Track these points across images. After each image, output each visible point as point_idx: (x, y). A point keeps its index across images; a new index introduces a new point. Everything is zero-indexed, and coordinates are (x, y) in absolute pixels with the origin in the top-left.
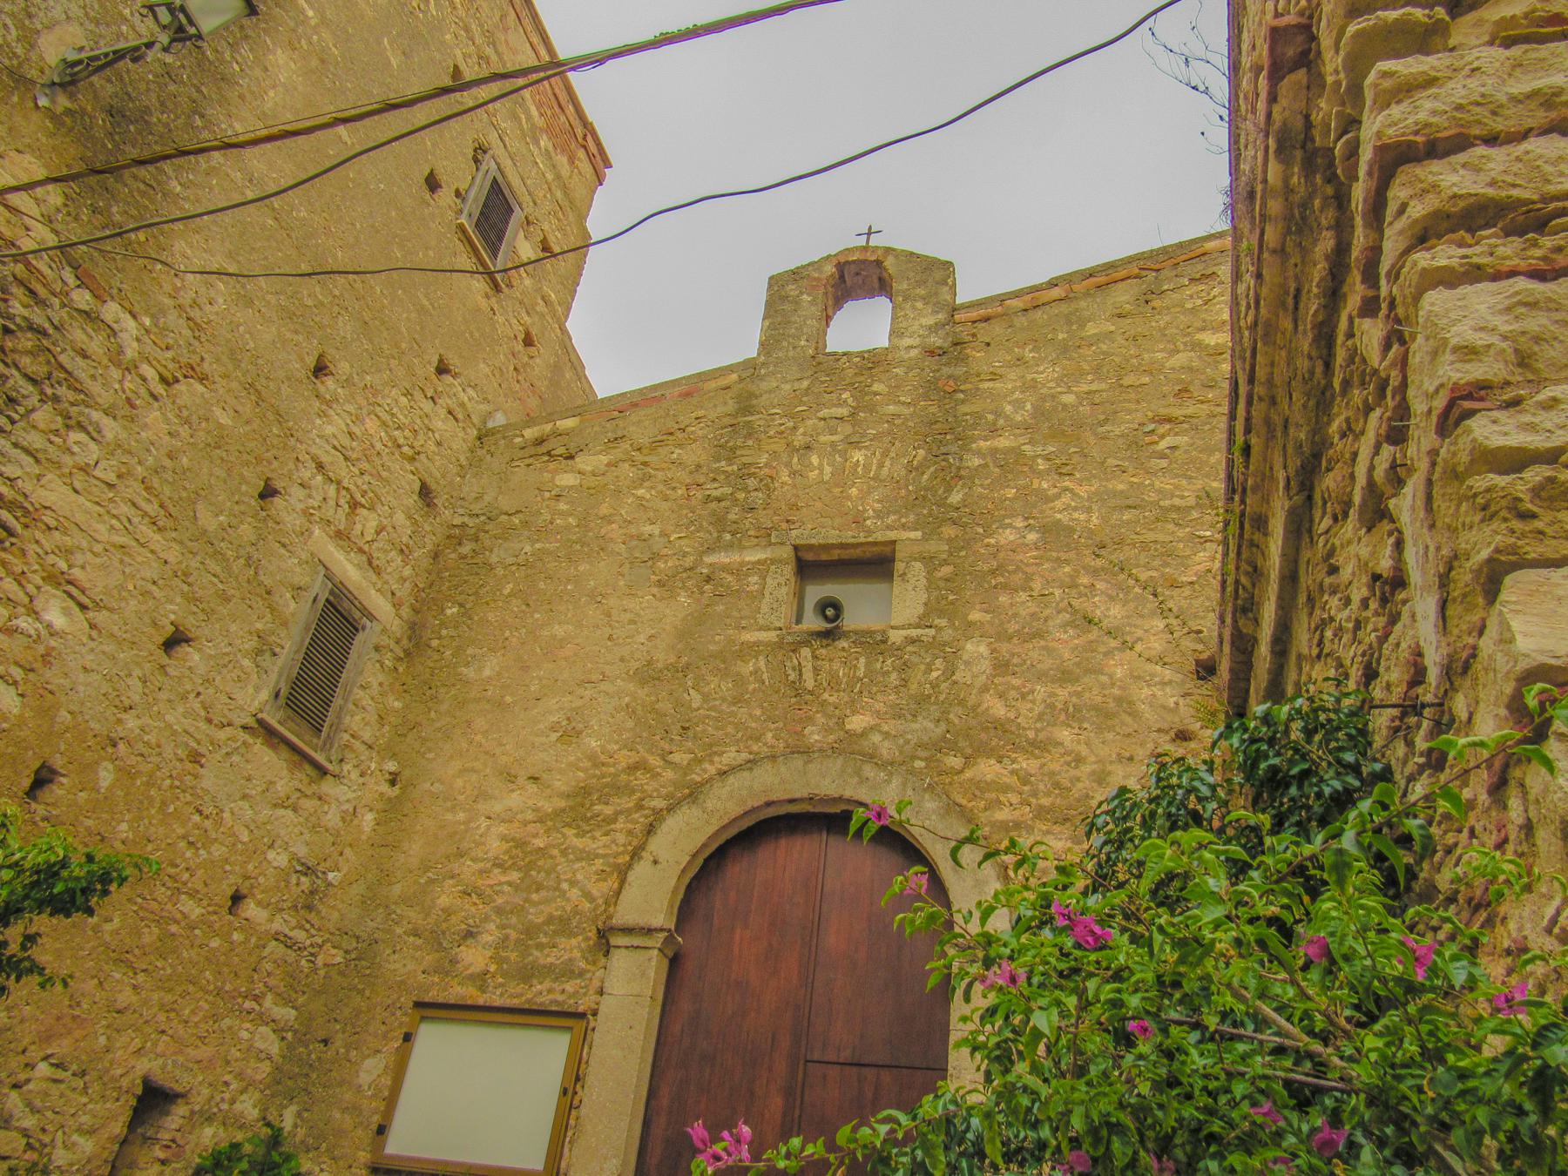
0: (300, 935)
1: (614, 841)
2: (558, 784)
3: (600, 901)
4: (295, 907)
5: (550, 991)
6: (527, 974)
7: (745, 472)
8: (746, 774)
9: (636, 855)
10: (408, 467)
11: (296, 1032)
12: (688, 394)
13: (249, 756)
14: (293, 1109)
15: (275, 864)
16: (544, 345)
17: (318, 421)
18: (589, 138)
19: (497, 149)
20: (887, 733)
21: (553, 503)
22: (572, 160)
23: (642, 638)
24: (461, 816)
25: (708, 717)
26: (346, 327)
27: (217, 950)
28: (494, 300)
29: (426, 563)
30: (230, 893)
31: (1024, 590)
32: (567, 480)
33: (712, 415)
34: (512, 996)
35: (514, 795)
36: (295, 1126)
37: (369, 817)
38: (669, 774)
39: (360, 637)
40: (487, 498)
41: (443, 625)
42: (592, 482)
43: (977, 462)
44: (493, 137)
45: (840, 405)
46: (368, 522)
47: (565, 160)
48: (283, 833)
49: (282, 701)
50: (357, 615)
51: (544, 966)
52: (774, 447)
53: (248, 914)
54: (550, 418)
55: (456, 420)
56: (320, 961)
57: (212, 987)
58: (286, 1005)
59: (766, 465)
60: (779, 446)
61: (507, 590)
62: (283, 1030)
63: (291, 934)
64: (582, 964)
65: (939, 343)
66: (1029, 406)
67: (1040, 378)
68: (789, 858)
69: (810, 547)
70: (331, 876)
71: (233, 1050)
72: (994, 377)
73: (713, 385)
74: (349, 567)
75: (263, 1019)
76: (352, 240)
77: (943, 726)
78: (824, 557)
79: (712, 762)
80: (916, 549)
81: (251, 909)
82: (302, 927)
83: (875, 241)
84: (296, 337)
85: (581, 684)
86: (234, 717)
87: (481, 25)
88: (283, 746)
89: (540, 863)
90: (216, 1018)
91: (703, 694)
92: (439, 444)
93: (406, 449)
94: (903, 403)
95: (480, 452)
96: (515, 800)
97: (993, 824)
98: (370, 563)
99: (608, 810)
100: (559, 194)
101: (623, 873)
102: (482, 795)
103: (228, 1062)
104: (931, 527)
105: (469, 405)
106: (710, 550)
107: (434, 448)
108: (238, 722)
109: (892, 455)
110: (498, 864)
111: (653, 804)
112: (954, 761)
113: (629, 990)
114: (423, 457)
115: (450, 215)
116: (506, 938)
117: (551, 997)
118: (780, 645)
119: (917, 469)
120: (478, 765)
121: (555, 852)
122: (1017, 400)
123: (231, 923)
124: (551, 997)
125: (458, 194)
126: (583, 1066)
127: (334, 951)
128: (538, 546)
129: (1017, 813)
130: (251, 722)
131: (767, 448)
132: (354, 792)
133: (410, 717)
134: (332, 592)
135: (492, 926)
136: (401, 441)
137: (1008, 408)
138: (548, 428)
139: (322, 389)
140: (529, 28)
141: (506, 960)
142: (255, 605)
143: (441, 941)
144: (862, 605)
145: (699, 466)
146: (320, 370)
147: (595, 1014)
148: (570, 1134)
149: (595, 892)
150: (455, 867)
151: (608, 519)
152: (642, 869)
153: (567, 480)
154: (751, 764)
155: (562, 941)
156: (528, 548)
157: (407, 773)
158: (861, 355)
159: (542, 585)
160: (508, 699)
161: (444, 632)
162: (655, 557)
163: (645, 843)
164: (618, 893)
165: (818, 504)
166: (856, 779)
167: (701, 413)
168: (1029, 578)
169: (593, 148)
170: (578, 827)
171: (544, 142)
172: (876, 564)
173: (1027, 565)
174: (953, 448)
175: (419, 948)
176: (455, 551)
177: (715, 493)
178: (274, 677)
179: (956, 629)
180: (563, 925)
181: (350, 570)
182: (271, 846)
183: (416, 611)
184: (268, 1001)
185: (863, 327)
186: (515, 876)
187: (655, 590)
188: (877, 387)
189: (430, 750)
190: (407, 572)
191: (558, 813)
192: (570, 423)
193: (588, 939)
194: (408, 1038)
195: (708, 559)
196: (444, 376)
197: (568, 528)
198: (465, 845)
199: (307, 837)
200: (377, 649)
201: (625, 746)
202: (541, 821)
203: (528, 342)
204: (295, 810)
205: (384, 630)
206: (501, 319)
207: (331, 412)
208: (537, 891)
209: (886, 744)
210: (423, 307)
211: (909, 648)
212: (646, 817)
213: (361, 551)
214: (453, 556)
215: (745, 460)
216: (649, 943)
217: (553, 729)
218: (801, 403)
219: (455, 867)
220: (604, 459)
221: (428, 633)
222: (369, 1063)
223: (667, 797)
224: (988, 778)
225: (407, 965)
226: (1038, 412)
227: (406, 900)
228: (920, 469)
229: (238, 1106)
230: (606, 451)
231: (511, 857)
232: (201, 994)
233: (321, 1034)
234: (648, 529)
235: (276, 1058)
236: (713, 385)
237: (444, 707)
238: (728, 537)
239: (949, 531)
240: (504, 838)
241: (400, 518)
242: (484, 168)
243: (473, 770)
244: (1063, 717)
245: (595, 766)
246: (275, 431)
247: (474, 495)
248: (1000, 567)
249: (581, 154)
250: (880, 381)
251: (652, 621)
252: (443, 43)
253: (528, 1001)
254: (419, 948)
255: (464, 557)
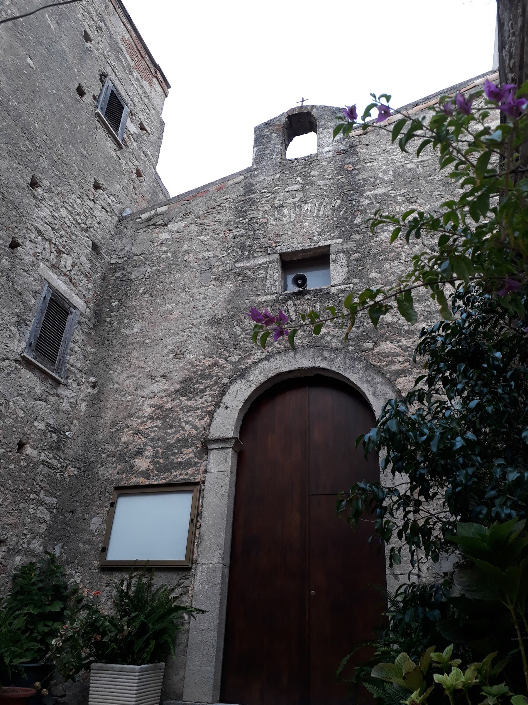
0: (55, 462)
1: (206, 401)
2: (175, 377)
3: (202, 429)
4: (50, 448)
5: (181, 474)
6: (169, 468)
7: (252, 222)
8: (267, 362)
9: (217, 406)
10: (85, 234)
11: (57, 509)
12: (221, 188)
13: (19, 374)
14: (60, 545)
15: (38, 428)
16: (144, 173)
17: (36, 210)
18: (158, 72)
19: (112, 76)
20: (334, 335)
21: (159, 248)
22: (151, 84)
23: (210, 305)
24: (130, 398)
25: (246, 338)
26: (44, 163)
27: (13, 470)
28: (119, 152)
29: (99, 282)
30: (17, 442)
31: (396, 260)
32: (165, 236)
33: (233, 197)
34: (162, 479)
35: (155, 385)
36: (61, 553)
37: (84, 404)
38: (229, 366)
39: (70, 317)
40: (127, 249)
41: (111, 310)
42: (177, 235)
43: (367, 202)
44: (109, 69)
45: (296, 184)
46: (67, 261)
47: (147, 84)
48: (41, 413)
49: (33, 348)
50: (67, 306)
51: (177, 463)
52: (265, 208)
53: (27, 452)
54: (153, 208)
55: (107, 212)
56: (66, 475)
57: (12, 488)
58: (51, 496)
59: (262, 217)
60: (268, 207)
61: (141, 291)
62: (51, 508)
63: (50, 462)
64: (196, 460)
65: (343, 147)
66: (391, 172)
67: (395, 157)
68: (293, 400)
69: (287, 253)
70: (67, 433)
71: (27, 518)
72: (372, 160)
73: (232, 182)
74: (60, 282)
75: (40, 502)
76: (42, 118)
77: (361, 329)
78: (295, 258)
79: (249, 359)
80: (340, 248)
81: (28, 450)
82: (55, 458)
83: (305, 104)
84: (19, 166)
85: (183, 330)
86: (9, 355)
87: (96, 11)
88: (36, 370)
89: (171, 415)
90: (17, 503)
91: (242, 328)
92: (99, 223)
93: (82, 225)
94: (328, 179)
95: (120, 228)
96: (155, 387)
97: (391, 372)
98: (71, 281)
99: (202, 386)
100: (146, 101)
101: (211, 415)
102: (140, 387)
103: (25, 524)
104: (347, 236)
105: (112, 204)
106: (239, 261)
107: (97, 225)
108: (12, 358)
109: (324, 204)
110: (150, 418)
111: (223, 381)
112: (370, 345)
113: (219, 468)
114: (91, 229)
115: (92, 108)
116: (157, 452)
117: (181, 477)
118: (277, 301)
119: (337, 209)
120: (135, 373)
121: (177, 409)
122: (385, 170)
123: (19, 457)
124: (181, 477)
125: (94, 97)
126: (200, 508)
127: (72, 469)
128: (154, 268)
129: (403, 366)
130: (17, 357)
131: (262, 209)
132: (74, 393)
133: (100, 355)
134: (53, 295)
135: (149, 448)
136: (80, 221)
137: (381, 175)
138: (153, 212)
139: (36, 194)
140: (121, 14)
141: (158, 463)
142: (14, 300)
143: (125, 458)
144: (314, 280)
145: (229, 222)
146: (34, 184)
147: (204, 482)
148: (196, 541)
149: (199, 426)
150: (129, 422)
151: (187, 252)
152: (221, 411)
153: (165, 236)
154: (268, 358)
155: (185, 451)
156: (149, 270)
157: (100, 382)
158: (304, 159)
159: (158, 287)
160: (147, 341)
161: (112, 314)
162: (212, 267)
163: (221, 399)
164: (210, 424)
165: (290, 233)
166: (320, 358)
167: (227, 197)
168: (398, 254)
169: (161, 79)
170: (188, 396)
171: (135, 74)
172: (320, 258)
173: (397, 248)
174: (355, 197)
175: (113, 463)
176: (113, 275)
177: (238, 234)
178: (27, 336)
179: (364, 283)
180: (185, 443)
181: (61, 285)
182: (36, 419)
183: (97, 305)
184: (42, 494)
185: (303, 146)
186: (158, 423)
187: (214, 283)
188: (313, 173)
189: (111, 369)
190: (90, 286)
191: (177, 391)
192: (164, 209)
193: (198, 447)
194: (113, 505)
195: (238, 265)
196: (98, 190)
197: (168, 258)
198: (133, 411)
199: (53, 414)
200: (79, 323)
201: (207, 356)
202: (169, 395)
203: (139, 174)
204: (46, 401)
205: (82, 314)
206: (124, 162)
207: (42, 205)
208: (170, 428)
209: (334, 340)
210: (83, 154)
211: (341, 295)
212: (220, 387)
213: (65, 275)
214: (112, 278)
215: (251, 216)
216: (227, 446)
217: (171, 352)
218: (277, 185)
219: (129, 422)
220: (182, 224)
221: (103, 315)
222: (94, 520)
223: (229, 377)
224: (386, 351)
225: (110, 471)
226: (396, 174)
227: (106, 441)
228: (339, 209)
229: (32, 546)
230: (182, 220)
231: (156, 414)
232: (7, 491)
233: (71, 508)
234: (207, 255)
235: (49, 522)
236: (232, 182)
237: (116, 348)
238: (247, 253)
239: (356, 237)
240: (152, 406)
241: (83, 259)
242: (106, 85)
243: (133, 376)
244: (422, 318)
245: (193, 367)
246: (14, 213)
247: (120, 248)
248: (383, 250)
249: (155, 81)
250: (315, 170)
251: (214, 297)
252: (77, 18)
253: (170, 480)
254: (113, 463)
255: (118, 278)
